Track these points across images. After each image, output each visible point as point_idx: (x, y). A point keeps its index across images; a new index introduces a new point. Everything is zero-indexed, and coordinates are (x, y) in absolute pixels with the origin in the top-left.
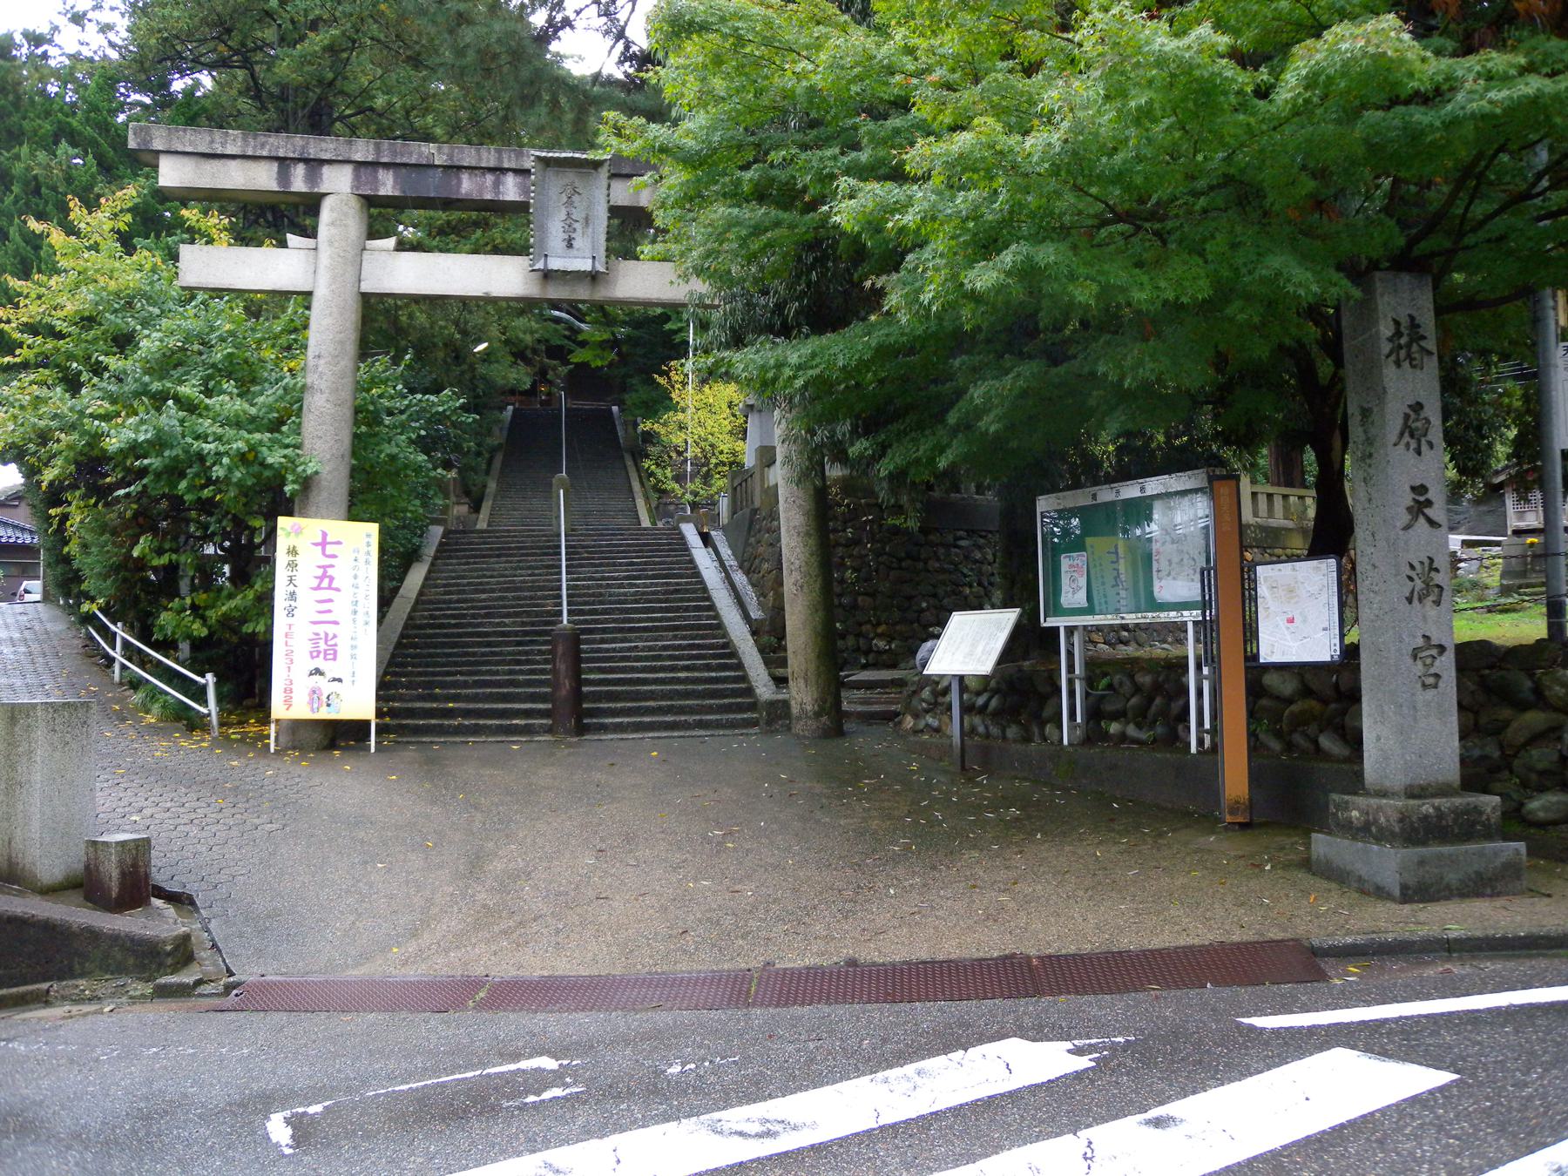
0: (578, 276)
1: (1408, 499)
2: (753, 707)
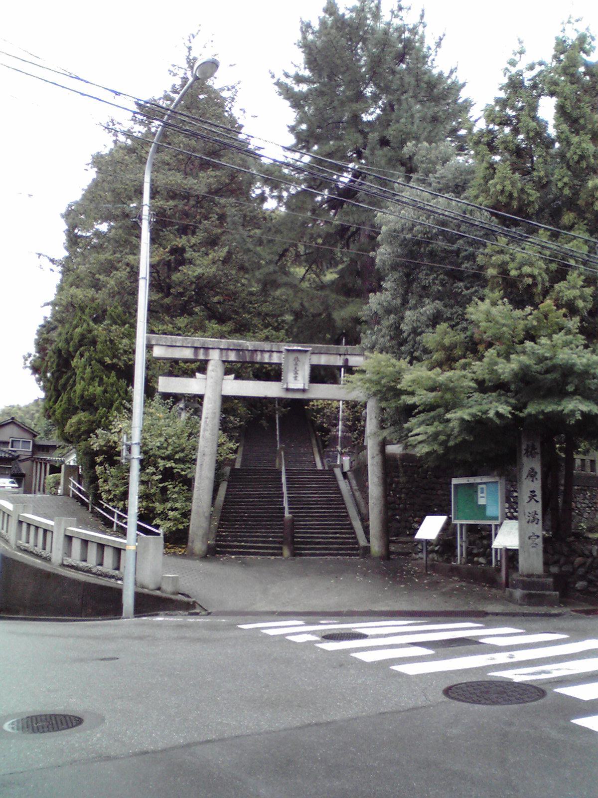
0: (298, 390)
1: (529, 494)
2: (357, 549)
